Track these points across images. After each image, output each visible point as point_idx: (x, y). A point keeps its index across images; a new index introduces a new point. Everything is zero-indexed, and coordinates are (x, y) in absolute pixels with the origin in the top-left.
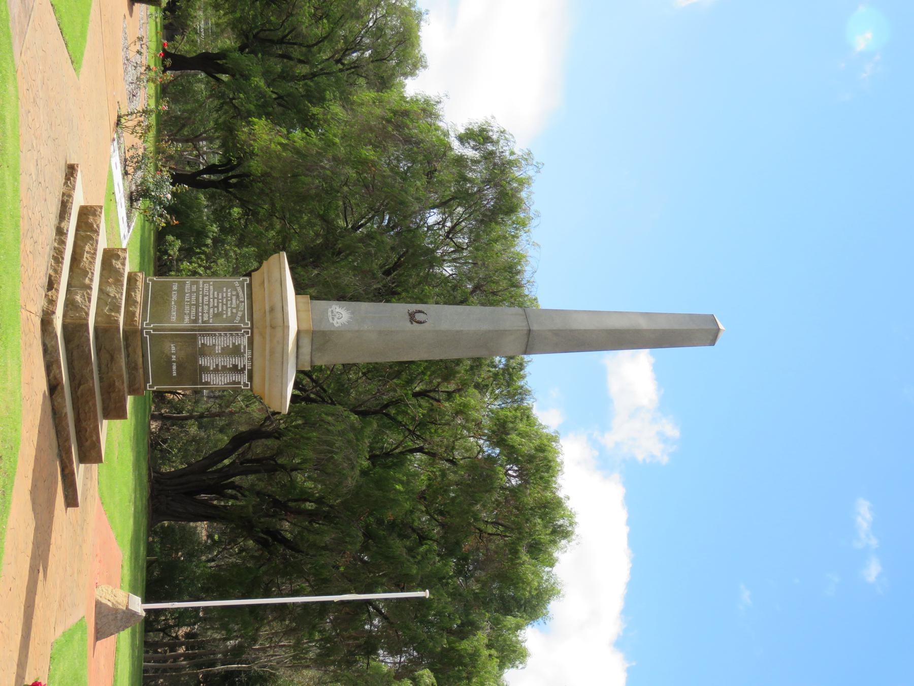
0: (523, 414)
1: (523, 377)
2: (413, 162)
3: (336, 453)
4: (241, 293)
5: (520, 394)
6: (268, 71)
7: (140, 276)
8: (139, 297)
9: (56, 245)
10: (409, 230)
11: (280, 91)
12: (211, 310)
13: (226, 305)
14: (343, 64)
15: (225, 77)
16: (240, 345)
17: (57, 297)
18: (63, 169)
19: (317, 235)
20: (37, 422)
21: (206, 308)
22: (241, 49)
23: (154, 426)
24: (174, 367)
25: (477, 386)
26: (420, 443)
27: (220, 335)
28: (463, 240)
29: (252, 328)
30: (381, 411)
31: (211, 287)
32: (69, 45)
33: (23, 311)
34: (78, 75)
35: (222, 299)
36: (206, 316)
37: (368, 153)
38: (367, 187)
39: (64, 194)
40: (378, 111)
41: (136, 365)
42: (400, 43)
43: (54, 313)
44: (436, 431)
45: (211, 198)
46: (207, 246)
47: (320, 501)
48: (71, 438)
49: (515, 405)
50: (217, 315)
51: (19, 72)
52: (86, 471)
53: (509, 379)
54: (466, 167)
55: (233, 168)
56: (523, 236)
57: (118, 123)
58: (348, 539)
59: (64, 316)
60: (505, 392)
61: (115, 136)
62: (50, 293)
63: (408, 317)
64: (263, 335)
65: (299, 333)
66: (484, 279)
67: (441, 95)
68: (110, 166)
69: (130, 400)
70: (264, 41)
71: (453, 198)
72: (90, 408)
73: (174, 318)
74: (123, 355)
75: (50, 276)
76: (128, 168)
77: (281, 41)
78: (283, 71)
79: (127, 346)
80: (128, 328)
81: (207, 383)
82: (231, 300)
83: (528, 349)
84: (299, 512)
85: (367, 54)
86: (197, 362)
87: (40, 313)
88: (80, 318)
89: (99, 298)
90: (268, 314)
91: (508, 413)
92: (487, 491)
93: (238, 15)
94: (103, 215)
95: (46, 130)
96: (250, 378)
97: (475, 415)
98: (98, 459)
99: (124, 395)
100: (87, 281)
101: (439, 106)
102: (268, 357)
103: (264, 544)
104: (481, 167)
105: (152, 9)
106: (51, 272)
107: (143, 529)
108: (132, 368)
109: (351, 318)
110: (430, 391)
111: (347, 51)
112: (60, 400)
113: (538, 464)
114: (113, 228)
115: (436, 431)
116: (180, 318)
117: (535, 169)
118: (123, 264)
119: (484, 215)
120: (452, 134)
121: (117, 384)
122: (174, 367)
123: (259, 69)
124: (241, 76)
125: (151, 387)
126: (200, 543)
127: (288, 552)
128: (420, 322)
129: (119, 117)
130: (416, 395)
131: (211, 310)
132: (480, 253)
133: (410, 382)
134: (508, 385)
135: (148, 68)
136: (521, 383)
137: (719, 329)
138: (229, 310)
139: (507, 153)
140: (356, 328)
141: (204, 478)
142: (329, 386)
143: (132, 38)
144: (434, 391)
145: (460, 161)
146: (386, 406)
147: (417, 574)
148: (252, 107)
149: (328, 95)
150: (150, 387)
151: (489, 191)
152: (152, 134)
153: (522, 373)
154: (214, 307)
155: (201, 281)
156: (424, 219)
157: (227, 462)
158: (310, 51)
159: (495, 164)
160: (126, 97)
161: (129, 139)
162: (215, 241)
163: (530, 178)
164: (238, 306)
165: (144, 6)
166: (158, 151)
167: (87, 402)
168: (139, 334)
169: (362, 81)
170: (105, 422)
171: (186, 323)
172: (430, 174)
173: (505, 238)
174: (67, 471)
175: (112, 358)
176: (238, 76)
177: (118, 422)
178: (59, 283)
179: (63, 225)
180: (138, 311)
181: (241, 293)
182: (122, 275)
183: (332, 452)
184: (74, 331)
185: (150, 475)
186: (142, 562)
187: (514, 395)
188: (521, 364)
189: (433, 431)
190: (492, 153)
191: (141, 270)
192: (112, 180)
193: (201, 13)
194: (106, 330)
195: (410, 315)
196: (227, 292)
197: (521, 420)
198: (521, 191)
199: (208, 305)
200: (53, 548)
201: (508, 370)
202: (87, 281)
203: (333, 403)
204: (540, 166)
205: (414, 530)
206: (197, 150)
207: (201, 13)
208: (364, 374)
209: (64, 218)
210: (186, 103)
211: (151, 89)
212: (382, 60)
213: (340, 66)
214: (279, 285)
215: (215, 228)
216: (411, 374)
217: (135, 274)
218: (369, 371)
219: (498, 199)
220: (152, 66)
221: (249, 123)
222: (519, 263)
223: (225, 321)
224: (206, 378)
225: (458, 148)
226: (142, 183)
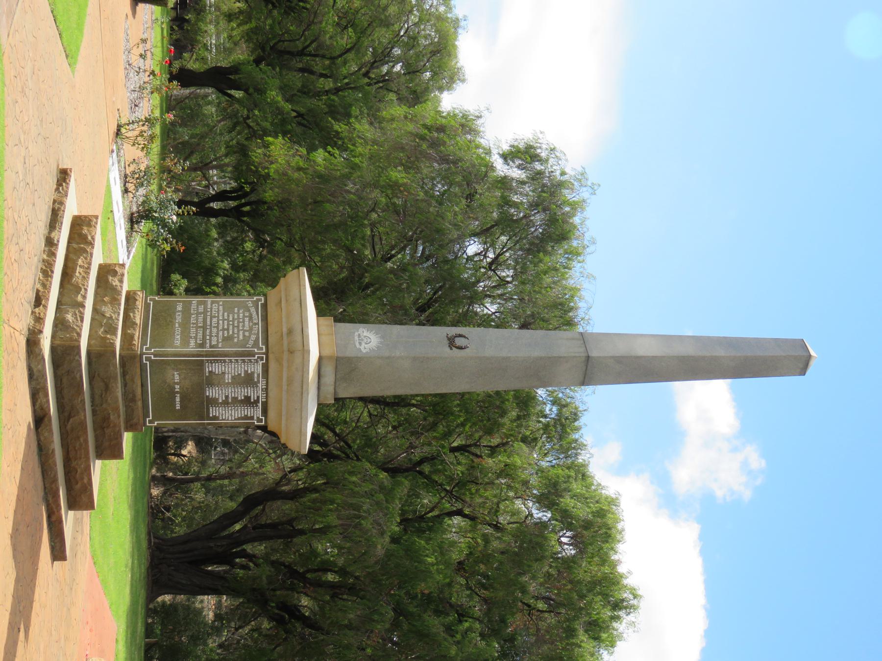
0: (577, 472)
1: (578, 429)
2: (451, 185)
3: (364, 518)
4: (254, 314)
5: (574, 448)
6: (286, 86)
7: (140, 295)
8: (138, 318)
9: (45, 257)
10: (446, 261)
11: (302, 110)
12: (221, 333)
13: (238, 327)
14: (369, 78)
15: (238, 94)
16: (253, 373)
17: (45, 314)
18: (55, 174)
19: (342, 268)
20: (21, 457)
22: (257, 62)
23: (155, 492)
24: (178, 399)
25: (524, 440)
26: (459, 505)
27: (231, 361)
28: (507, 273)
29: (267, 353)
30: (412, 469)
31: (221, 308)
32: (64, 35)
33: (6, 326)
34: (73, 72)
36: (214, 339)
37: (397, 175)
38: (397, 213)
39: (54, 201)
40: (411, 127)
41: (134, 396)
42: (434, 53)
43: (41, 332)
44: (477, 491)
45: (222, 229)
46: (216, 284)
47: (342, 572)
48: (58, 481)
49: (569, 461)
50: (228, 339)
51: (6, 55)
52: (78, 522)
53: (562, 429)
54: (511, 189)
55: (246, 195)
56: (576, 267)
57: (118, 133)
58: (376, 617)
59: (53, 337)
60: (557, 447)
61: (115, 148)
62: (37, 310)
63: (446, 342)
64: (279, 361)
65: (320, 359)
66: (533, 315)
67: (482, 109)
68: (108, 181)
69: (128, 438)
70: (282, 53)
71: (497, 224)
72: (81, 445)
73: (178, 343)
74: (119, 385)
75: (38, 291)
76: (129, 185)
77: (302, 53)
78: (303, 86)
79: (124, 374)
80: (124, 353)
81: (215, 418)
82: (244, 322)
83: (586, 380)
84: (319, 584)
85: (398, 68)
86: (203, 391)
87: (25, 332)
88: (71, 339)
89: (93, 319)
90: (285, 338)
91: (560, 471)
92: (537, 560)
93: (253, 24)
94: (99, 226)
95: (36, 126)
96: (265, 412)
97: (523, 475)
98: (90, 505)
99: (120, 430)
100: (80, 298)
101: (479, 122)
102: (285, 387)
103: (279, 621)
104: (527, 189)
105: (157, 9)
106: (39, 286)
107: (142, 600)
108: (129, 399)
109: (381, 343)
110: (470, 446)
111: (373, 65)
112: (46, 434)
113: (596, 530)
114: (110, 251)
115: (477, 491)
116: (185, 341)
117: (590, 190)
118: (121, 281)
119: (532, 244)
120: (495, 151)
121: (112, 417)
122: (178, 399)
123: (277, 82)
124: (255, 91)
125: (152, 423)
126: (206, 624)
127: (307, 631)
128: (460, 348)
129: (119, 127)
130: (453, 450)
131: (221, 333)
132: (528, 287)
133: (447, 435)
134: (561, 438)
135: (153, 73)
136: (575, 436)
137: (810, 356)
138: (241, 333)
139: (558, 173)
140: (387, 354)
141: (212, 544)
142: (354, 441)
143: (134, 40)
144: (475, 445)
145: (504, 183)
146: (421, 462)
147: (457, 654)
148: (267, 125)
149: (355, 111)
150: (150, 422)
151: (536, 219)
152: (156, 147)
153: (576, 424)
154: (223, 330)
155: (209, 301)
156: (463, 249)
157: (237, 527)
158: (333, 63)
159: (544, 185)
160: (128, 106)
161: (131, 152)
162: (226, 279)
163: (584, 201)
164: (251, 329)
165: (148, 6)
166: (164, 170)
167: (78, 438)
168: (138, 359)
169: (392, 96)
170: (98, 463)
171: (192, 347)
172: (470, 197)
173: (556, 270)
174: (54, 518)
175: (107, 388)
176: (251, 90)
177: (115, 461)
178: (48, 299)
179: (53, 235)
180: (137, 334)
182: (119, 293)
183: (359, 517)
184: (64, 354)
185: (149, 541)
186: (141, 640)
187: (568, 449)
188: (575, 414)
189: (473, 491)
190: (540, 173)
191: (144, 287)
192: (111, 197)
193: (212, 27)
194: (100, 355)
195: (449, 339)
196: (238, 313)
197: (576, 479)
198: (574, 215)
199: (217, 327)
200: (36, 605)
201: (559, 420)
202: (80, 298)
203: (358, 460)
204: (596, 187)
205: (451, 605)
206: (207, 180)
207: (211, 28)
208: (394, 428)
210: (194, 127)
211: (156, 99)
212: (414, 72)
213: (366, 80)
214: (298, 305)
215: (226, 265)
216: (448, 426)
217: (135, 293)
218: (400, 425)
219: (547, 225)
220: (157, 71)
221: (266, 146)
223: (235, 345)
224: (213, 412)
225: (501, 169)
226: (144, 202)
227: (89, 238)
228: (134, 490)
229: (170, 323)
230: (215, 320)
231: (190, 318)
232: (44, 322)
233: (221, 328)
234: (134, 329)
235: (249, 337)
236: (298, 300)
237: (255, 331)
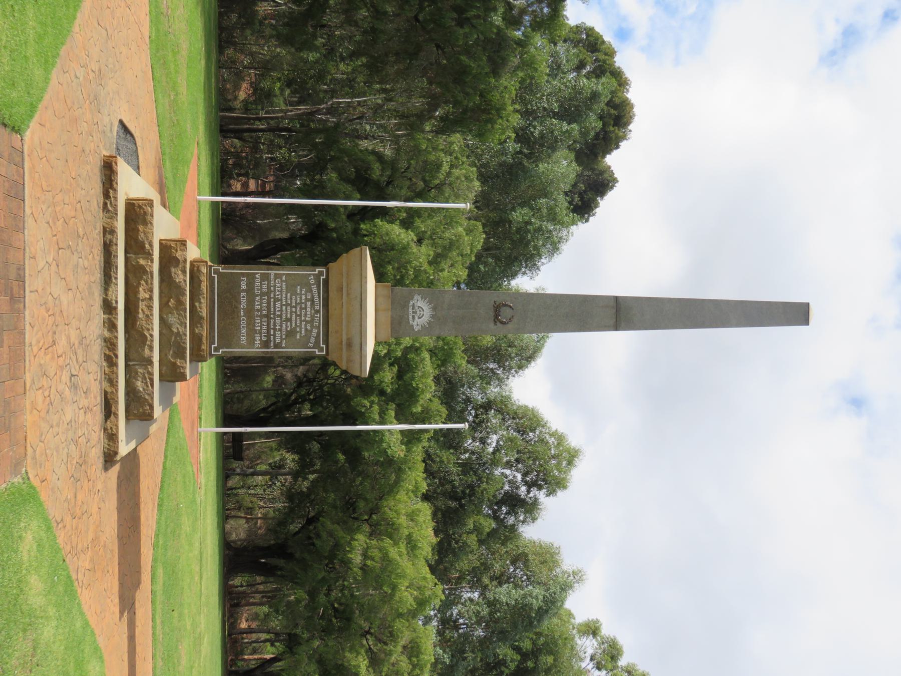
4: (316, 297)
21: (278, 321)
35: (295, 307)
36: (278, 334)
50: (291, 334)
73: (244, 339)
75: (106, 393)
107: (214, 56)
116: (251, 342)
138: (303, 323)
154: (287, 305)
171: (256, 350)
181: (316, 297)
196: (301, 294)
199: (280, 316)
209: (110, 278)
214: (358, 306)
222: (627, 84)
227: (147, 246)
229: (235, 310)
230: (278, 304)
231: (254, 300)
232: (117, 438)
233: (284, 318)
235: (311, 331)
236: (359, 299)
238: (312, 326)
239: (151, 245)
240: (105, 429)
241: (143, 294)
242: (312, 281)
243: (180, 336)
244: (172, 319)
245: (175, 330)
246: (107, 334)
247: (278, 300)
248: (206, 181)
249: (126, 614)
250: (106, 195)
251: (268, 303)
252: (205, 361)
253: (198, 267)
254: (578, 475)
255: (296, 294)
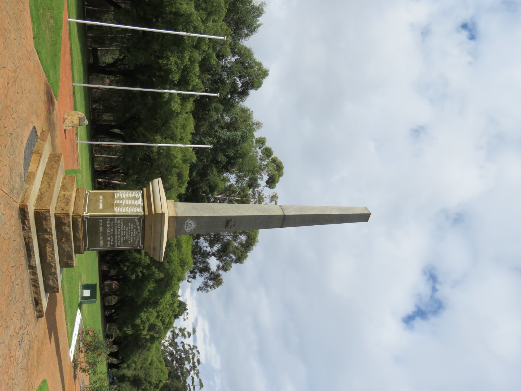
8: (81, 235)
21: (119, 237)
35: (128, 231)
36: (119, 242)
39: (25, 238)
50: (125, 242)
75: (35, 298)
100: (53, 270)
109: (196, 227)
116: (105, 245)
154: (123, 236)
164: (136, 236)
181: (138, 228)
196: (131, 226)
199: (120, 235)
209: (31, 256)
227: (49, 230)
228: (85, 96)
234: (80, 242)
235: (136, 240)
237: (138, 237)
238: (136, 238)
239: (51, 229)
240: (36, 310)
241: (48, 249)
242: (137, 221)
243: (70, 252)
244: (65, 246)
245: (66, 250)
246: (32, 277)
247: (119, 229)
248: (74, 11)
249: (53, 336)
250: (23, 223)
251: (114, 230)
252: (83, 253)
253: (76, 219)
254: (266, 82)
255: (128, 226)
